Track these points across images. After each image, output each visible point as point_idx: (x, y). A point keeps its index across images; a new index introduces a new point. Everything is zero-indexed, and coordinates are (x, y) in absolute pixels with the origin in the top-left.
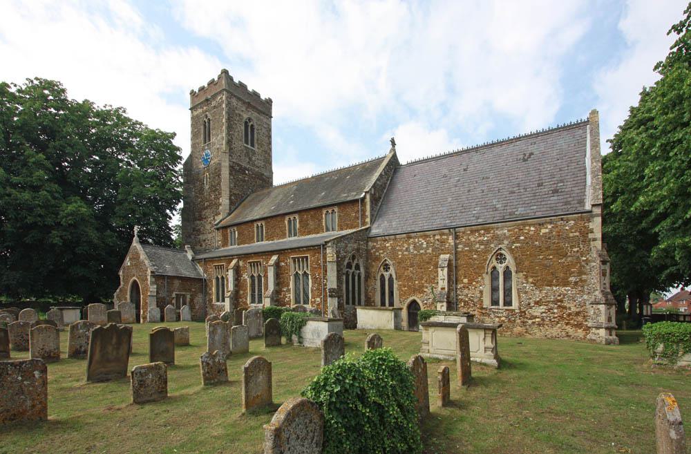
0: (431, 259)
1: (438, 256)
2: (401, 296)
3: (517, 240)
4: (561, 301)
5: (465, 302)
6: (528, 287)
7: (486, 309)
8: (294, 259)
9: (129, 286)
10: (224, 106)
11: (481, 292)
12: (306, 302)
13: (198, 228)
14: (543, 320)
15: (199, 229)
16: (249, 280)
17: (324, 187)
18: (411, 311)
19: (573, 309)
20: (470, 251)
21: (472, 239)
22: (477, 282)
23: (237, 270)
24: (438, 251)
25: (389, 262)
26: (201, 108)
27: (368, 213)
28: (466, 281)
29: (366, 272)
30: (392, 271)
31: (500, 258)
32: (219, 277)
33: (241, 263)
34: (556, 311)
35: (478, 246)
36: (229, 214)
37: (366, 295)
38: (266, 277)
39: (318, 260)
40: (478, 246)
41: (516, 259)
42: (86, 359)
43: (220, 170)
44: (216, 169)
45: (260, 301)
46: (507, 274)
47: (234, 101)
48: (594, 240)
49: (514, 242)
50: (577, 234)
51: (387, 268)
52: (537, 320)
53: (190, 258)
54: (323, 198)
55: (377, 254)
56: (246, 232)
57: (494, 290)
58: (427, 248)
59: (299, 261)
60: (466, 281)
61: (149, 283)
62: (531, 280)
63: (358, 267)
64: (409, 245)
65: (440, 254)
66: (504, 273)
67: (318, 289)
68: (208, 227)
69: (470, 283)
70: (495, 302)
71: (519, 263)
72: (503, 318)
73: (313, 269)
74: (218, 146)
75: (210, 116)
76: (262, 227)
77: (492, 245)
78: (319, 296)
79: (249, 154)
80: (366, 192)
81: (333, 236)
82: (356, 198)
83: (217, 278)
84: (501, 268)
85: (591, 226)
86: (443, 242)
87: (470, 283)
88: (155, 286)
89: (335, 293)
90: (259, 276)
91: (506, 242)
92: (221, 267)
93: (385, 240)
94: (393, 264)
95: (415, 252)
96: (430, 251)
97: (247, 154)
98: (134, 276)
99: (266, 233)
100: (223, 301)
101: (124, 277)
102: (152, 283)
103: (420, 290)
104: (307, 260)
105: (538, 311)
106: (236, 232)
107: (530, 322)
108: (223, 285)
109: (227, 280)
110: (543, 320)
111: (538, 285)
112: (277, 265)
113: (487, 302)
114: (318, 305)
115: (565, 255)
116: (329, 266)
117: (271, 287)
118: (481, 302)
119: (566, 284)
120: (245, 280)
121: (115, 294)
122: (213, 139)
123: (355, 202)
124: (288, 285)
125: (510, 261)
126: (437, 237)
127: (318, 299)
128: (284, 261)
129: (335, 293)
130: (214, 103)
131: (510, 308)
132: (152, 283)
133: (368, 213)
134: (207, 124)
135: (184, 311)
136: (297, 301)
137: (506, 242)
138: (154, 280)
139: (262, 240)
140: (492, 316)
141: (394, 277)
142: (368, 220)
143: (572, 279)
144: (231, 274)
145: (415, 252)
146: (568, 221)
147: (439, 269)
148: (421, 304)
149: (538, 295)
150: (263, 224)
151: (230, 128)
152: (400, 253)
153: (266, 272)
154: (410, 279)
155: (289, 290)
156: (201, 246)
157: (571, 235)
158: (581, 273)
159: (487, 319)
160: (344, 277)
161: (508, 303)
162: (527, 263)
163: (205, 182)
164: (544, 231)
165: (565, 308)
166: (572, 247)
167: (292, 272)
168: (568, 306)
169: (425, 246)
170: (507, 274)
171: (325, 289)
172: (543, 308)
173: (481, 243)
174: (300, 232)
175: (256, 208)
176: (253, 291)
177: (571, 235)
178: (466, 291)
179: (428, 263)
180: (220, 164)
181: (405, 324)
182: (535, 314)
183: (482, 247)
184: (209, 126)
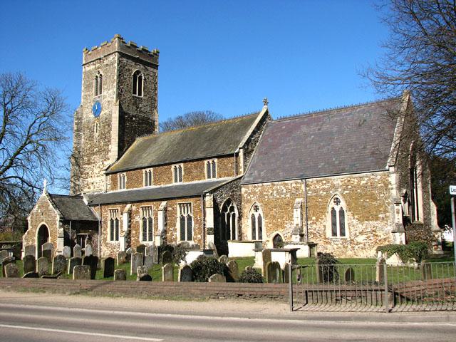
0: (289, 202)
1: (294, 200)
2: (267, 231)
3: (346, 188)
4: (375, 231)
5: (314, 234)
6: (355, 222)
7: (328, 239)
8: (180, 204)
9: (38, 230)
10: (116, 65)
11: (325, 226)
12: (190, 238)
13: (86, 171)
14: (364, 245)
15: (88, 173)
16: (141, 223)
17: (206, 138)
18: (276, 243)
19: (383, 237)
20: (316, 196)
21: (318, 187)
22: (322, 219)
23: (130, 213)
24: (295, 196)
25: (258, 204)
26: (93, 64)
27: (241, 164)
28: (314, 218)
29: (239, 213)
30: (260, 211)
31: (337, 202)
32: (114, 219)
33: (134, 208)
34: (371, 238)
35: (321, 192)
36: (118, 159)
37: (240, 232)
38: (157, 219)
39: (200, 205)
40: (321, 192)
41: (346, 201)
42: (55, 259)
43: (110, 121)
44: (106, 119)
45: (151, 239)
46: (342, 212)
47: (125, 60)
48: (392, 189)
49: (344, 190)
50: (382, 185)
51: (256, 209)
52: (361, 245)
53: (87, 203)
54: (205, 150)
55: (249, 197)
56: (134, 177)
57: (334, 224)
58: (286, 194)
59: (184, 206)
60: (314, 218)
61: (58, 226)
62: (356, 217)
63: (232, 209)
64: (273, 191)
65: (296, 198)
66: (340, 211)
67: (199, 228)
68: (96, 171)
69: (317, 220)
70: (334, 234)
71: (348, 204)
72: (340, 245)
73: (195, 213)
74: (109, 99)
75: (101, 73)
76: (150, 173)
77: (331, 192)
78: (200, 234)
79: (136, 101)
80: (240, 148)
81: (224, 181)
82: (232, 152)
83: (112, 221)
84: (337, 209)
85: (390, 179)
86: (297, 189)
87: (317, 220)
88: (62, 229)
89: (209, 231)
90: (150, 218)
91: (340, 190)
92: (116, 211)
93: (255, 187)
94: (261, 206)
95: (278, 197)
96: (288, 196)
97: (135, 104)
98: (43, 221)
99: (155, 178)
100: (117, 239)
101: (32, 222)
102: (60, 227)
103: (282, 226)
104: (190, 205)
105: (361, 239)
106: (126, 177)
107: (357, 247)
108: (117, 226)
109: (122, 222)
110: (364, 245)
111: (361, 220)
112: (165, 209)
113: (329, 233)
114: (199, 240)
115: (376, 200)
116: (207, 210)
117: (161, 227)
118: (325, 233)
119: (377, 219)
120: (137, 222)
121: (24, 236)
122: (104, 93)
123: (232, 155)
124: (175, 225)
125: (343, 204)
126: (293, 185)
127: (199, 236)
128: (171, 207)
129: (209, 231)
130: (106, 62)
131: (344, 237)
132: (60, 227)
133: (241, 164)
134: (99, 79)
135: (88, 249)
136: (183, 238)
137: (340, 190)
138: (61, 224)
139: (150, 185)
140: (333, 244)
141: (262, 215)
142: (242, 170)
143: (381, 216)
144: (125, 218)
145: (278, 197)
146: (376, 176)
147: (295, 210)
148: (282, 237)
149: (361, 227)
150: (152, 171)
151: (120, 83)
152: (266, 197)
153: (156, 214)
154: (274, 217)
155: (175, 230)
156: (89, 188)
157: (379, 185)
158: (386, 211)
159: (329, 246)
160: (220, 218)
161: (343, 234)
162: (353, 205)
163: (95, 130)
164: (363, 182)
165: (377, 236)
166: (380, 193)
167: (179, 215)
168: (379, 234)
169: (285, 191)
170: (342, 212)
171: (204, 228)
172: (364, 237)
173: (324, 190)
174: (185, 178)
175: (145, 155)
176: (145, 230)
177: (379, 185)
178: (314, 226)
179: (287, 205)
180: (110, 115)
181: (318, 281)
182: (359, 241)
183: (325, 193)
184: (101, 83)
